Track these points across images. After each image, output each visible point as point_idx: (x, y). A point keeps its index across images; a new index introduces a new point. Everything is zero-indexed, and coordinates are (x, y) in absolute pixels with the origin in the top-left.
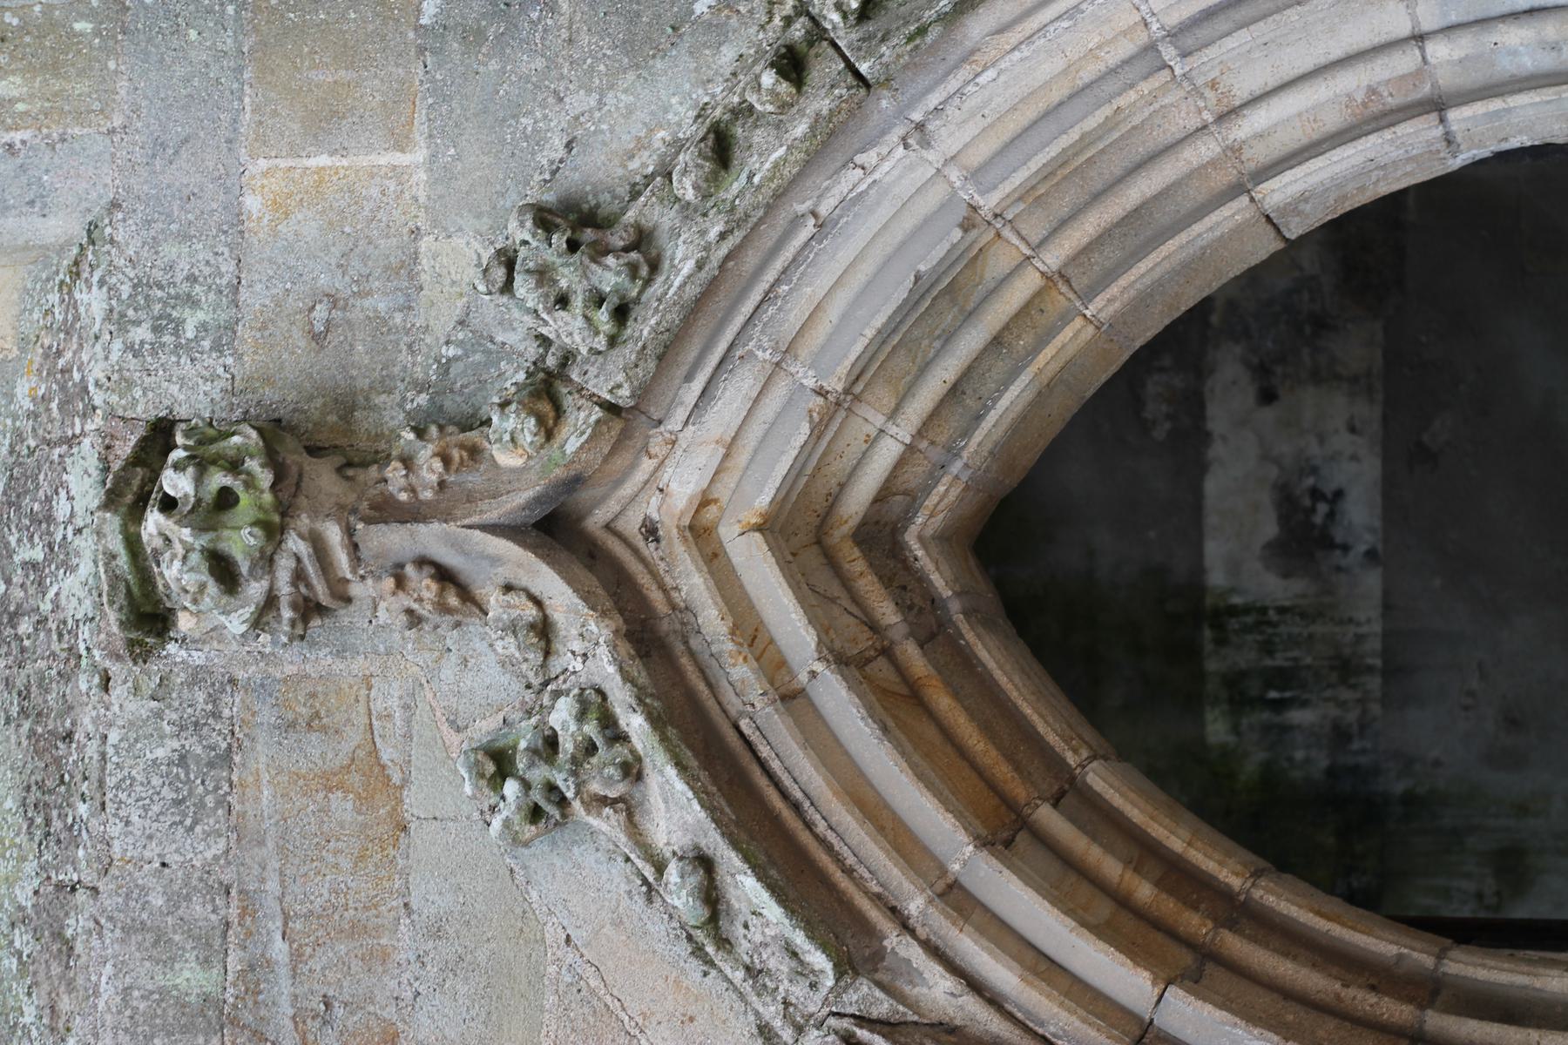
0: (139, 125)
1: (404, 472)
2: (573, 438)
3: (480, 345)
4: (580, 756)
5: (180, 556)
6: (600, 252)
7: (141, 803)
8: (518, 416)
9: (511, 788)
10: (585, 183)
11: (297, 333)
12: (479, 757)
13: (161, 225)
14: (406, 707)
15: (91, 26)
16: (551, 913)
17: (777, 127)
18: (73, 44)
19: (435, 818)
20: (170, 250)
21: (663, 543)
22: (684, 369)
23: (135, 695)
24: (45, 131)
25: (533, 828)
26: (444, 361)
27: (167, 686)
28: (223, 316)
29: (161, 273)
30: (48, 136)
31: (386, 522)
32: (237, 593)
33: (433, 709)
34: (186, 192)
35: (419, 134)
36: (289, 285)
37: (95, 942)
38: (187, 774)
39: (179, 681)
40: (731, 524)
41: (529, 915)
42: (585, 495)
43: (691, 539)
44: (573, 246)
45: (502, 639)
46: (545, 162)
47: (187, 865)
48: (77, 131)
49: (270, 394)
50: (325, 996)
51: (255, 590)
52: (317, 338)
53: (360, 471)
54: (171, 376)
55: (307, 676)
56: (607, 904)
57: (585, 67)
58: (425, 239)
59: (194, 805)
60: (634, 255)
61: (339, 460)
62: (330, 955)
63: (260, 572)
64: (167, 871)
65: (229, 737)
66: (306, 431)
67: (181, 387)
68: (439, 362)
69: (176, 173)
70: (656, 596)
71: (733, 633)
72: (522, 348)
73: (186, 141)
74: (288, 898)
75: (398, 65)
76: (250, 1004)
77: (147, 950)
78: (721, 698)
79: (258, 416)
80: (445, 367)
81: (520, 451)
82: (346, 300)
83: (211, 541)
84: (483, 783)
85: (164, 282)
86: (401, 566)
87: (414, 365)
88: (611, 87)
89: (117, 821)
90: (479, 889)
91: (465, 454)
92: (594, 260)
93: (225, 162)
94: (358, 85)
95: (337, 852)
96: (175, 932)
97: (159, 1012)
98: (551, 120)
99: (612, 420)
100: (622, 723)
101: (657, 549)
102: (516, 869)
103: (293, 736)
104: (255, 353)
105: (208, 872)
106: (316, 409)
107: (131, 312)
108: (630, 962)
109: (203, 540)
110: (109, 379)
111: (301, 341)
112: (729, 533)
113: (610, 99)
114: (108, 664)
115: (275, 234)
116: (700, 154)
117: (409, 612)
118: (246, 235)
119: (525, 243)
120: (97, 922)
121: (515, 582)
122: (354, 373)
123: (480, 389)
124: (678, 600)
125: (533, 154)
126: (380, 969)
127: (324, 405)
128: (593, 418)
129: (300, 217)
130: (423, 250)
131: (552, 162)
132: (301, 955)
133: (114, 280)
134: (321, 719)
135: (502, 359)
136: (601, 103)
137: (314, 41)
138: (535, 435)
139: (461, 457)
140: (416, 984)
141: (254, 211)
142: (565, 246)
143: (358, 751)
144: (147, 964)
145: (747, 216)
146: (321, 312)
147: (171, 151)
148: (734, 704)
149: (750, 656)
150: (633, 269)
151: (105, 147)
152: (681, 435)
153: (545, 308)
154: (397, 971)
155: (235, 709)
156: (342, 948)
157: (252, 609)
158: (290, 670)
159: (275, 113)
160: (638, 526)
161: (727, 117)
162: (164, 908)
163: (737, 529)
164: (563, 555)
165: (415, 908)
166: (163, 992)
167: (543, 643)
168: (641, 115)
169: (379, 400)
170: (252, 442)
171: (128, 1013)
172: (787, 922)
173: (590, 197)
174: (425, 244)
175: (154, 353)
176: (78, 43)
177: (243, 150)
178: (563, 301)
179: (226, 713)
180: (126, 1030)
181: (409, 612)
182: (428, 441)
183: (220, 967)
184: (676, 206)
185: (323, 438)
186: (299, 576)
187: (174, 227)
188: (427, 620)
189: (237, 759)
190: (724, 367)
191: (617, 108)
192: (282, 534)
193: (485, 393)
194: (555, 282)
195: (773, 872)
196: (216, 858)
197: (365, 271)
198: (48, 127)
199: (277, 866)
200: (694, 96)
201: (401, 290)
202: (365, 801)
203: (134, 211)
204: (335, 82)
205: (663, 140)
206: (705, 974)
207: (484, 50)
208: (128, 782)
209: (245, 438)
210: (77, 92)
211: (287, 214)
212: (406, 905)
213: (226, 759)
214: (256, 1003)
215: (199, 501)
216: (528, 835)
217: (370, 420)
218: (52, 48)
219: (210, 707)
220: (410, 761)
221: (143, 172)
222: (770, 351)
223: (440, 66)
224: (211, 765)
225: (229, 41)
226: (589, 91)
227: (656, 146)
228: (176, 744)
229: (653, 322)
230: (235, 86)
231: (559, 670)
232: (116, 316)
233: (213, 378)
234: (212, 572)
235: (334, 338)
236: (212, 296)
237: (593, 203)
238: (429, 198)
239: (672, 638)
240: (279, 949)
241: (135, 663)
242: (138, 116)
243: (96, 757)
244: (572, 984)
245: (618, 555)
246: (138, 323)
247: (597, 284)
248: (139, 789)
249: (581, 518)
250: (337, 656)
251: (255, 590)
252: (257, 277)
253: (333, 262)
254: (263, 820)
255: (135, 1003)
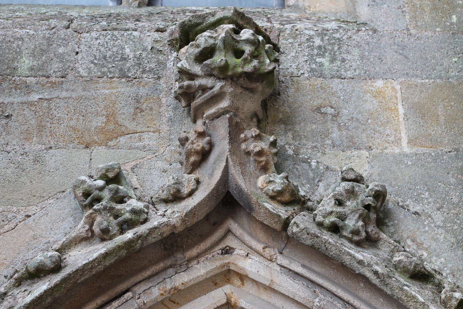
0: (412, 40)
1: (254, 135)
2: (271, 206)
3: (317, 176)
4: (114, 211)
5: (212, 35)
6: (365, 218)
7: (105, 43)
8: (282, 183)
9: (101, 183)
10: (398, 220)
11: (320, 101)
12: (116, 170)
13: (367, 49)
14: (144, 147)
15: (455, 21)
16: (42, 208)
17: (434, 300)
18: (446, 15)
19: (91, 159)
20: (356, 52)
21: (221, 256)
22: (308, 265)
23: (154, 41)
24: (406, 5)
25: (81, 194)
26: (309, 161)
27: (158, 53)
28: (327, 72)
29: (346, 49)
30: (404, 6)
31: (229, 126)
32: (196, 62)
33: (143, 158)
34: (383, 58)
35: (415, 149)
36: (342, 98)
37: (44, 27)
38: (117, 61)
39: (160, 57)
40: (231, 289)
41: (42, 199)
42: (245, 221)
43: (223, 270)
44: (367, 207)
45: (173, 178)
46: (407, 203)
47: (76, 61)
48: (407, 17)
49: (291, 91)
50: (12, 115)
51: (197, 69)
52: (318, 109)
53: (256, 124)
54: (299, 53)
55: (160, 107)
56: (44, 233)
57: (455, 220)
58: (367, 153)
59: (103, 64)
60: (364, 234)
61: (261, 115)
62: (30, 117)
63: (205, 70)
64: (74, 54)
65: (133, 76)
66: (274, 105)
67: (294, 57)
68: (308, 159)
69: (391, 54)
70: (194, 252)
71: (175, 288)
72: (316, 194)
73: (406, 57)
74: (58, 100)
75: (449, 140)
76: (11, 86)
77: (39, 46)
78: (143, 283)
79: (281, 87)
80: (306, 161)
81: (265, 185)
82: (336, 121)
83: (219, 47)
84: (104, 171)
85: (341, 50)
86: (210, 136)
87: (307, 148)
88: (447, 231)
89: (98, 35)
90: (56, 178)
91: (263, 163)
92: (360, 216)
93: (398, 72)
94: (438, 125)
95: (78, 119)
96: (46, 57)
97: (11, 51)
98: (428, 205)
99: (280, 223)
100: (130, 231)
101: (218, 254)
102: (64, 194)
103: (132, 102)
104: (310, 85)
105: (72, 70)
106: (285, 109)
107: (327, 38)
108: (15, 243)
109: (219, 43)
110: (297, 30)
111: (316, 103)
112: (227, 288)
113: (440, 231)
114: (169, 31)
115: (366, 92)
116: (417, 264)
117: (187, 139)
118: (364, 81)
119: (367, 187)
120: (53, 28)
121: (201, 185)
122: (302, 124)
123: (296, 176)
124: (192, 263)
125: (411, 198)
126: (22, 137)
127: (287, 112)
128: (282, 215)
129: (374, 102)
130: (362, 151)
131: (408, 206)
132: (31, 105)
133: (341, 31)
134: (140, 112)
135: (311, 185)
136: (438, 227)
137: (457, 107)
138: (273, 190)
139: (262, 161)
140: (13, 152)
141: (376, 84)
142: (367, 203)
143: (124, 128)
144: (33, 47)
145: (387, 285)
146: (330, 111)
147: (401, 52)
148: (139, 289)
149: (164, 297)
150: (356, 232)
151: (401, 27)
152: (275, 264)
153: (336, 194)
154: (20, 144)
155: (146, 79)
156: (33, 122)
157: (188, 68)
158: (164, 100)
159: (422, 92)
160: (229, 245)
161: (436, 281)
162: (57, 52)
163: (228, 292)
164: (213, 203)
165: (49, 151)
166: (20, 53)
167: (171, 198)
168: (434, 245)
169: (290, 135)
170: (266, 67)
171: (12, 40)
172: (23, 305)
173: (392, 223)
174: (365, 153)
175: (309, 47)
176: (447, 17)
177: (404, 80)
178: (340, 203)
179: (145, 76)
180: (4, 39)
181: (187, 139)
182: (270, 147)
183: (29, 74)
184: (389, 258)
185: (271, 112)
186: (204, 89)
187: (367, 53)
188: (183, 149)
189: (123, 80)
190: (310, 283)
191: (437, 234)
192: (223, 79)
193: (294, 178)
194: (349, 199)
195: (49, 300)
196: (79, 72)
197: (350, 128)
198: (408, 6)
199: (73, 96)
200: (445, 269)
201: (342, 143)
202: (101, 130)
203: (373, 38)
204: (438, 115)
205: (423, 255)
206: (6, 277)
207: (459, 176)
208: (115, 39)
209: (268, 65)
210: (425, 17)
211: (375, 97)
212: (51, 148)
213: (123, 75)
214: (11, 88)
215: (238, 42)
216: (78, 192)
217: (280, 131)
218: (443, 8)
219: (147, 69)
220: (119, 149)
221: (391, 41)
222: (319, 305)
223: (450, 157)
224: (121, 70)
225: (453, 74)
226: (444, 222)
227: (419, 252)
228: (131, 56)
229: (330, 240)
230: (433, 76)
231: (158, 208)
232: (325, 32)
233: (298, 69)
234: (205, 49)
235: (318, 116)
236: (336, 68)
237: (389, 224)
238: (387, 154)
239: (173, 259)
240: (35, 97)
241: (168, 41)
242: (416, 40)
243: (127, 27)
244: (7, 217)
245: (215, 234)
246: (322, 40)
247: (348, 218)
248: (112, 43)
249: (233, 218)
250: (169, 119)
251: (197, 69)
252: (345, 85)
253: (354, 116)
254: (95, 90)
255: (16, 42)
